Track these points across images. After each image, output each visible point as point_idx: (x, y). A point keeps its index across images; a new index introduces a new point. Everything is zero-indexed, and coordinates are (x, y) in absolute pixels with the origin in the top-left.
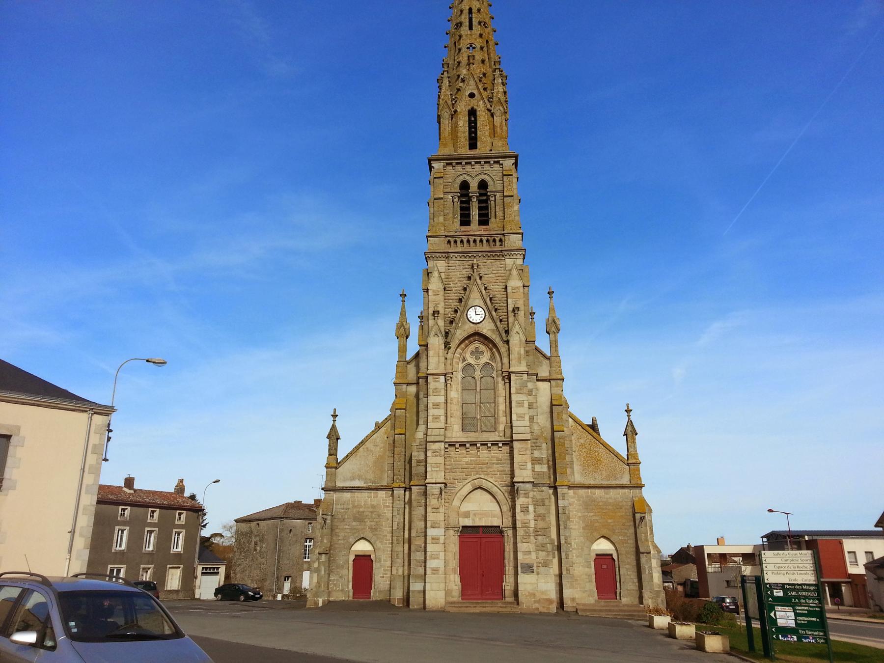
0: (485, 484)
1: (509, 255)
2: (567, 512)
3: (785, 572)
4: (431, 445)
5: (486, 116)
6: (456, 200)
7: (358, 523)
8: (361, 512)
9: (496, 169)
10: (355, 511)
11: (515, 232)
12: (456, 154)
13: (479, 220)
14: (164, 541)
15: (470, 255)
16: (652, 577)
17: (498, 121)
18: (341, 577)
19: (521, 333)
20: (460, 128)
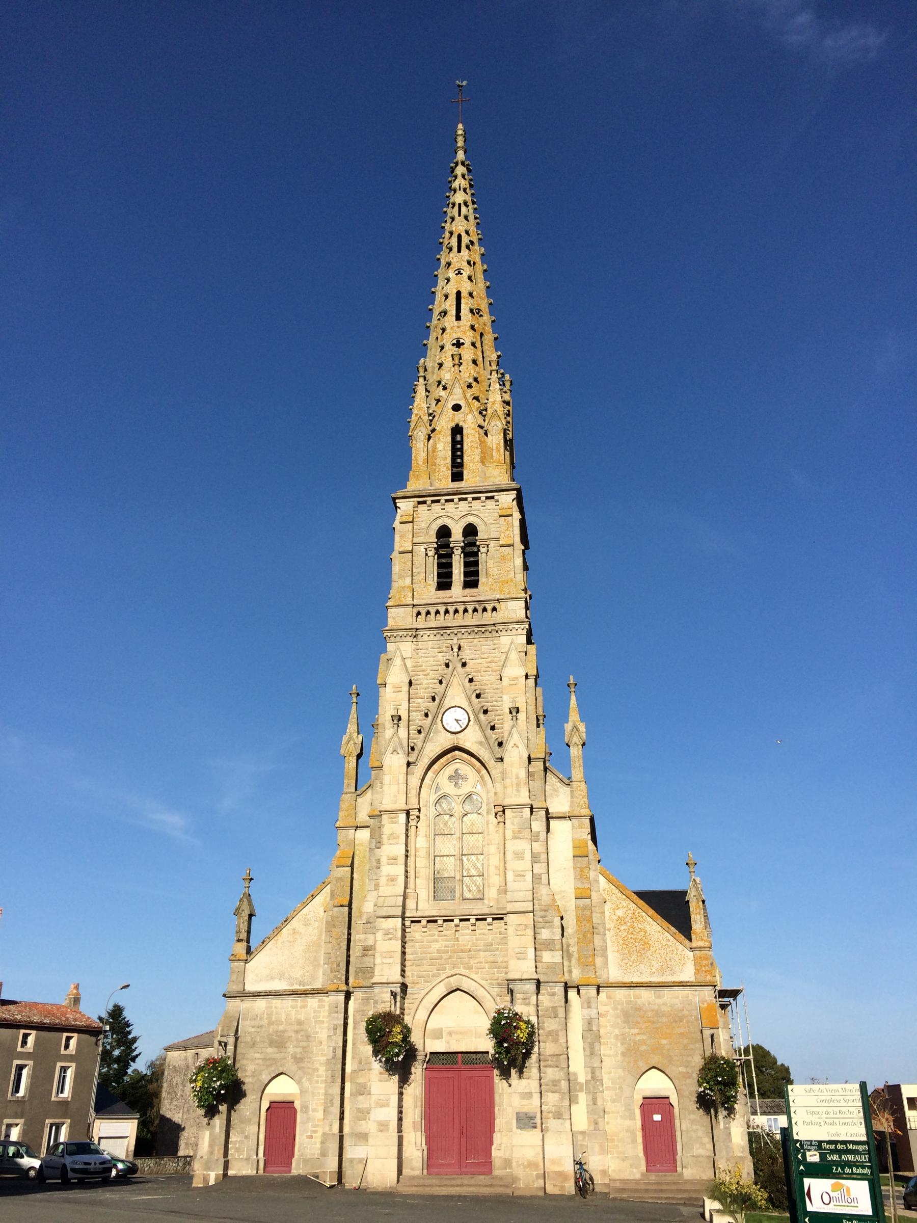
0: (466, 984)
1: (506, 631)
2: (594, 1028)
3: (821, 1121)
4: (382, 922)
5: (477, 435)
6: (430, 554)
7: (275, 1050)
8: (280, 1032)
9: (489, 507)
10: (271, 1030)
11: (514, 596)
12: (431, 488)
13: (464, 581)
14: (42, 1080)
15: (448, 632)
16: (730, 1134)
17: (494, 441)
18: (246, 1137)
19: (520, 746)
20: (439, 453)
